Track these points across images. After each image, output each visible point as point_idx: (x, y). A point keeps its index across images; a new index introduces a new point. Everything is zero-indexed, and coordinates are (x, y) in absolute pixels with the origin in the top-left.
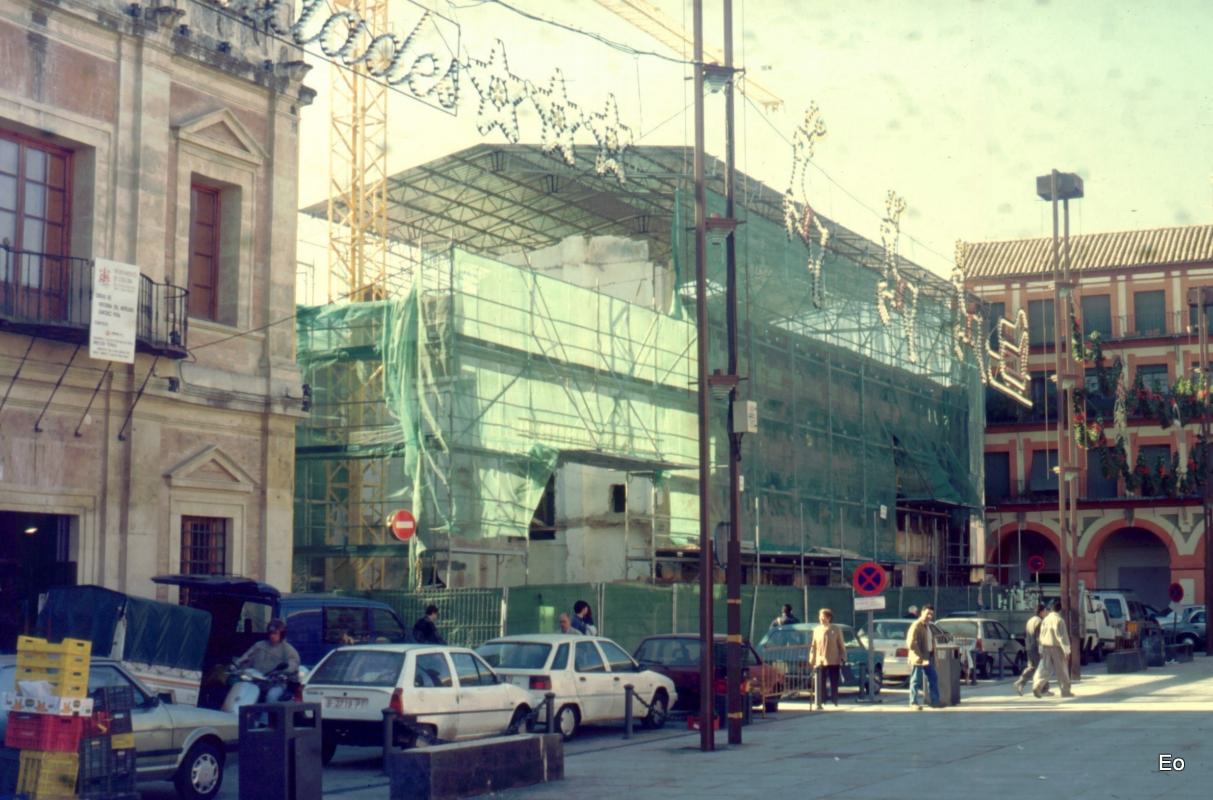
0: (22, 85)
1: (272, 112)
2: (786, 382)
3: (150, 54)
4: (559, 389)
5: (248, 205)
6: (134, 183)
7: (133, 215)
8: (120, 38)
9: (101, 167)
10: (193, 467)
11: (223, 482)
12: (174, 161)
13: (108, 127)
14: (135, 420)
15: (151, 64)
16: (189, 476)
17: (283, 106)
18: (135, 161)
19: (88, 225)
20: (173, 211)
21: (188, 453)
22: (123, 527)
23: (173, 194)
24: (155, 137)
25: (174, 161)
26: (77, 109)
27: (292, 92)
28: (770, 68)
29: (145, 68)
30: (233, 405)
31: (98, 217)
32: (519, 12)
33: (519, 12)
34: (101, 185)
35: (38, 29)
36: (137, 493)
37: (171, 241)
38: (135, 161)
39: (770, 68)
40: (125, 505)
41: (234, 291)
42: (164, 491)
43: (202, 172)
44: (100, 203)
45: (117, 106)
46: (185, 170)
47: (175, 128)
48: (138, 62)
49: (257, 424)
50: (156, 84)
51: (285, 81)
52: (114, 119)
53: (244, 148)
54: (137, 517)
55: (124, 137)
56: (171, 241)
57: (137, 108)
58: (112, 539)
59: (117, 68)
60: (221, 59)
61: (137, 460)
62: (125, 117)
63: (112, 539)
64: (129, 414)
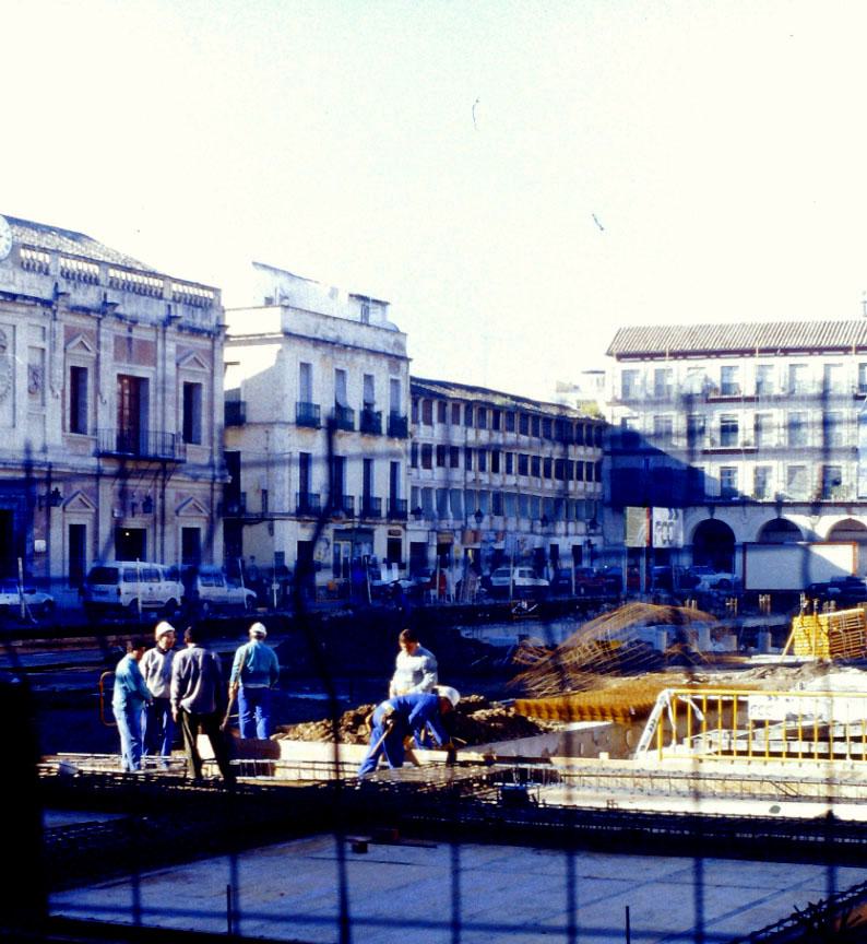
0: (125, 360)
1: (213, 347)
2: (554, 484)
3: (168, 335)
4: (501, 629)
5: (205, 391)
6: (164, 390)
7: (164, 404)
8: (157, 331)
9: (151, 386)
10: (185, 508)
11: (195, 513)
12: (177, 377)
13: (153, 368)
14: (166, 490)
15: (170, 340)
16: (186, 511)
17: (217, 344)
18: (164, 382)
19: (147, 410)
20: (177, 398)
21: (184, 501)
22: (163, 534)
23: (178, 391)
24: (171, 366)
25: (177, 377)
26: (143, 364)
27: (221, 338)
28: (602, 229)
29: (167, 343)
30: (201, 480)
31: (151, 408)
32: (249, 308)
33: (249, 308)
34: (151, 393)
35: (130, 335)
36: (168, 519)
37: (177, 413)
38: (164, 382)
39: (602, 229)
40: (163, 524)
41: (199, 430)
42: (176, 518)
43: (187, 380)
44: (151, 401)
45: (156, 359)
46: (181, 381)
47: (178, 365)
48: (164, 339)
49: (209, 486)
50: (171, 349)
51: (219, 333)
52: (155, 365)
53: (203, 366)
54: (168, 528)
55: (160, 372)
56: (177, 413)
57: (164, 359)
58: (158, 538)
59: (156, 343)
60: (196, 332)
61: (168, 506)
62: (160, 363)
63: (158, 538)
64: (164, 487)
